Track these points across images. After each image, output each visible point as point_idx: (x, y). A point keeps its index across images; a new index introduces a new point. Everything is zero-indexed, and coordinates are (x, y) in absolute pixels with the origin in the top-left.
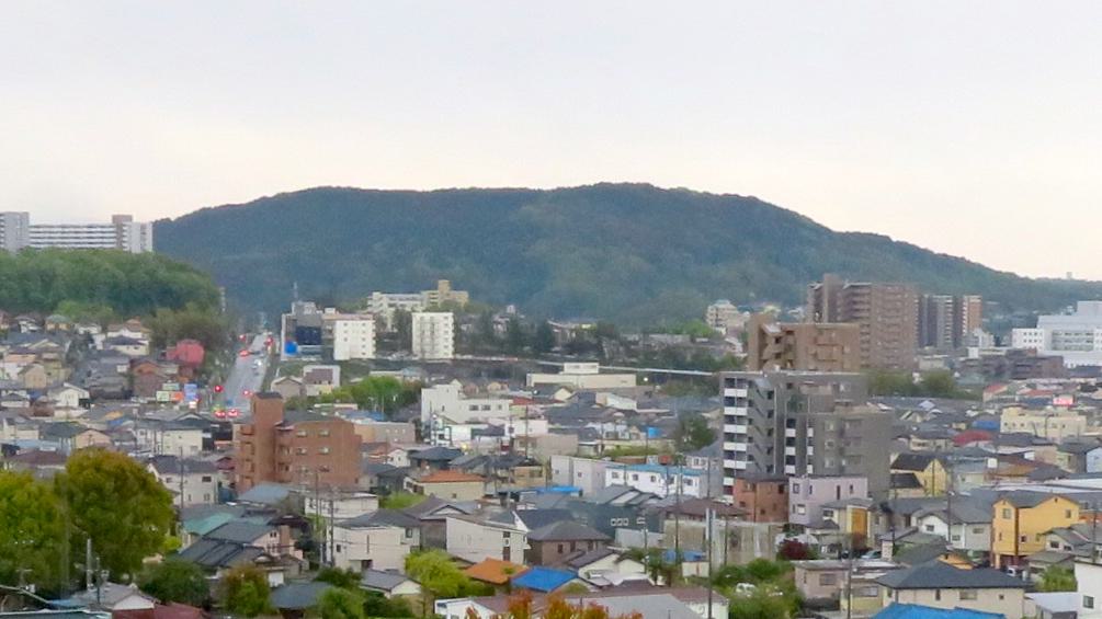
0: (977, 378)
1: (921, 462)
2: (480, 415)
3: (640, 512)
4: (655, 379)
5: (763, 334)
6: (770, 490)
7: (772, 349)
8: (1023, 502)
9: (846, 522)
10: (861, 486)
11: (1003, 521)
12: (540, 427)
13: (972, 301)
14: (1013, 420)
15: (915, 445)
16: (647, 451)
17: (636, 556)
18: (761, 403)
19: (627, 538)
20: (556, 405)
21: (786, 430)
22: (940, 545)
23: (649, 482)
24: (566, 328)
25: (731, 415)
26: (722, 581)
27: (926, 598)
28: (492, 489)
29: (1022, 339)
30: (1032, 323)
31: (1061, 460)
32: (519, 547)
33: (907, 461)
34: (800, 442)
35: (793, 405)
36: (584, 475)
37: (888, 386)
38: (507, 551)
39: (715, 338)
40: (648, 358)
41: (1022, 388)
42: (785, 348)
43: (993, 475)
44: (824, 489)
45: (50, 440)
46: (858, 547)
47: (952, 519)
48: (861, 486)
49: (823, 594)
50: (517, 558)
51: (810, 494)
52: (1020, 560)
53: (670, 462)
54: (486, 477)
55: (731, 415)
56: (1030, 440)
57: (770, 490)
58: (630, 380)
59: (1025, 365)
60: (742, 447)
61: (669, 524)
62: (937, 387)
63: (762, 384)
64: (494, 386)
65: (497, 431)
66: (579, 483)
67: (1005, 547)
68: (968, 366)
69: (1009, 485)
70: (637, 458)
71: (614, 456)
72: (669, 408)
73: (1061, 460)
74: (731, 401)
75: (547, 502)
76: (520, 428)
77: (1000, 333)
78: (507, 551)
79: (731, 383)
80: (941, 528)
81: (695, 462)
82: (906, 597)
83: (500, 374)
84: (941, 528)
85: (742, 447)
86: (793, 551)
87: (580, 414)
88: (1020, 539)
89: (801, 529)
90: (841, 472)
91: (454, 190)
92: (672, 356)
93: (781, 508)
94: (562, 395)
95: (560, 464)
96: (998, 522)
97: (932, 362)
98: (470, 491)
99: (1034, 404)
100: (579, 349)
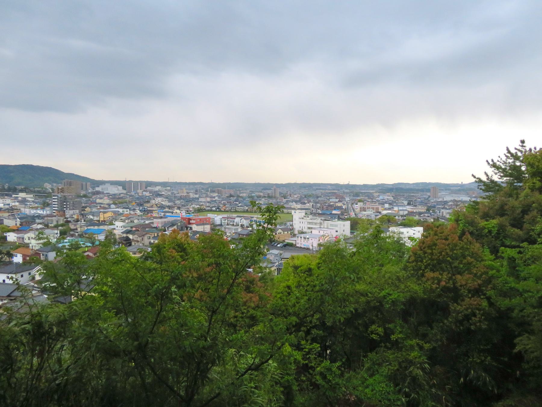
0: (90, 195)
1: (86, 207)
2: (4, 202)
3: (39, 217)
4: (36, 195)
5: (58, 188)
6: (62, 212)
7: (60, 191)
8: (104, 213)
9: (75, 217)
10: (77, 211)
11: (102, 216)
12: (17, 204)
13: (88, 184)
14: (98, 201)
15: (83, 205)
16: (38, 207)
17: (40, 224)
18: (60, 199)
19: (38, 221)
20: (327, 191)
21: (63, 202)
22: (92, 220)
23: (40, 212)
24: (20, 187)
25: (55, 201)
26: (56, 227)
27: (92, 227)
28: (10, 214)
29: (97, 189)
30: (98, 187)
31: (107, 206)
32: (18, 223)
33: (83, 207)
34: (67, 205)
35: (65, 199)
36: (28, 211)
37: (79, 196)
38: (16, 224)
39: (47, 189)
40: (34, 192)
41: (98, 196)
42: (62, 190)
43: (98, 209)
44: (71, 212)
45: (232, 196)
46: (77, 221)
47: (93, 216)
48: (77, 211)
49: (75, 228)
50: (18, 225)
51: (69, 213)
52: (104, 221)
53: (43, 209)
54: (9, 212)
55: (55, 201)
56: (102, 204)
57: (62, 212)
58: (32, 196)
59: (98, 193)
60: (56, 206)
61: (46, 218)
62: (85, 196)
63: (60, 196)
64: (6, 197)
65: (9, 204)
66: (26, 213)
67: (102, 219)
68: (89, 193)
69: (102, 210)
70: (36, 208)
71: (32, 208)
72: (41, 200)
73: (107, 206)
74: (54, 199)
75: (22, 216)
76: (13, 204)
77: (93, 188)
78: (16, 224)
79: (54, 196)
80: (91, 217)
81: (48, 209)
82: (89, 228)
83: (7, 195)
84: (91, 217)
85: (56, 206)
86: (68, 222)
87: (24, 201)
88: (104, 218)
89: (68, 218)
90: (74, 209)
91: (310, 183)
92: (39, 192)
93: (64, 215)
94: (20, 198)
95: (22, 209)
96: (101, 216)
97: (83, 193)
98: (6, 215)
99: (101, 198)
100: (22, 191)
